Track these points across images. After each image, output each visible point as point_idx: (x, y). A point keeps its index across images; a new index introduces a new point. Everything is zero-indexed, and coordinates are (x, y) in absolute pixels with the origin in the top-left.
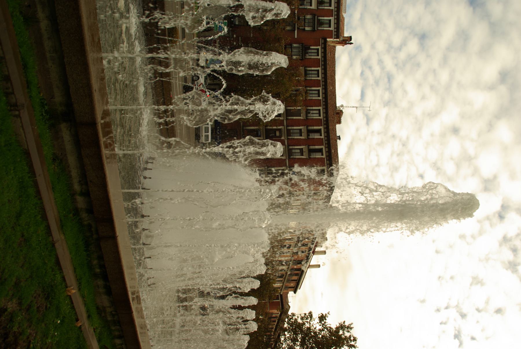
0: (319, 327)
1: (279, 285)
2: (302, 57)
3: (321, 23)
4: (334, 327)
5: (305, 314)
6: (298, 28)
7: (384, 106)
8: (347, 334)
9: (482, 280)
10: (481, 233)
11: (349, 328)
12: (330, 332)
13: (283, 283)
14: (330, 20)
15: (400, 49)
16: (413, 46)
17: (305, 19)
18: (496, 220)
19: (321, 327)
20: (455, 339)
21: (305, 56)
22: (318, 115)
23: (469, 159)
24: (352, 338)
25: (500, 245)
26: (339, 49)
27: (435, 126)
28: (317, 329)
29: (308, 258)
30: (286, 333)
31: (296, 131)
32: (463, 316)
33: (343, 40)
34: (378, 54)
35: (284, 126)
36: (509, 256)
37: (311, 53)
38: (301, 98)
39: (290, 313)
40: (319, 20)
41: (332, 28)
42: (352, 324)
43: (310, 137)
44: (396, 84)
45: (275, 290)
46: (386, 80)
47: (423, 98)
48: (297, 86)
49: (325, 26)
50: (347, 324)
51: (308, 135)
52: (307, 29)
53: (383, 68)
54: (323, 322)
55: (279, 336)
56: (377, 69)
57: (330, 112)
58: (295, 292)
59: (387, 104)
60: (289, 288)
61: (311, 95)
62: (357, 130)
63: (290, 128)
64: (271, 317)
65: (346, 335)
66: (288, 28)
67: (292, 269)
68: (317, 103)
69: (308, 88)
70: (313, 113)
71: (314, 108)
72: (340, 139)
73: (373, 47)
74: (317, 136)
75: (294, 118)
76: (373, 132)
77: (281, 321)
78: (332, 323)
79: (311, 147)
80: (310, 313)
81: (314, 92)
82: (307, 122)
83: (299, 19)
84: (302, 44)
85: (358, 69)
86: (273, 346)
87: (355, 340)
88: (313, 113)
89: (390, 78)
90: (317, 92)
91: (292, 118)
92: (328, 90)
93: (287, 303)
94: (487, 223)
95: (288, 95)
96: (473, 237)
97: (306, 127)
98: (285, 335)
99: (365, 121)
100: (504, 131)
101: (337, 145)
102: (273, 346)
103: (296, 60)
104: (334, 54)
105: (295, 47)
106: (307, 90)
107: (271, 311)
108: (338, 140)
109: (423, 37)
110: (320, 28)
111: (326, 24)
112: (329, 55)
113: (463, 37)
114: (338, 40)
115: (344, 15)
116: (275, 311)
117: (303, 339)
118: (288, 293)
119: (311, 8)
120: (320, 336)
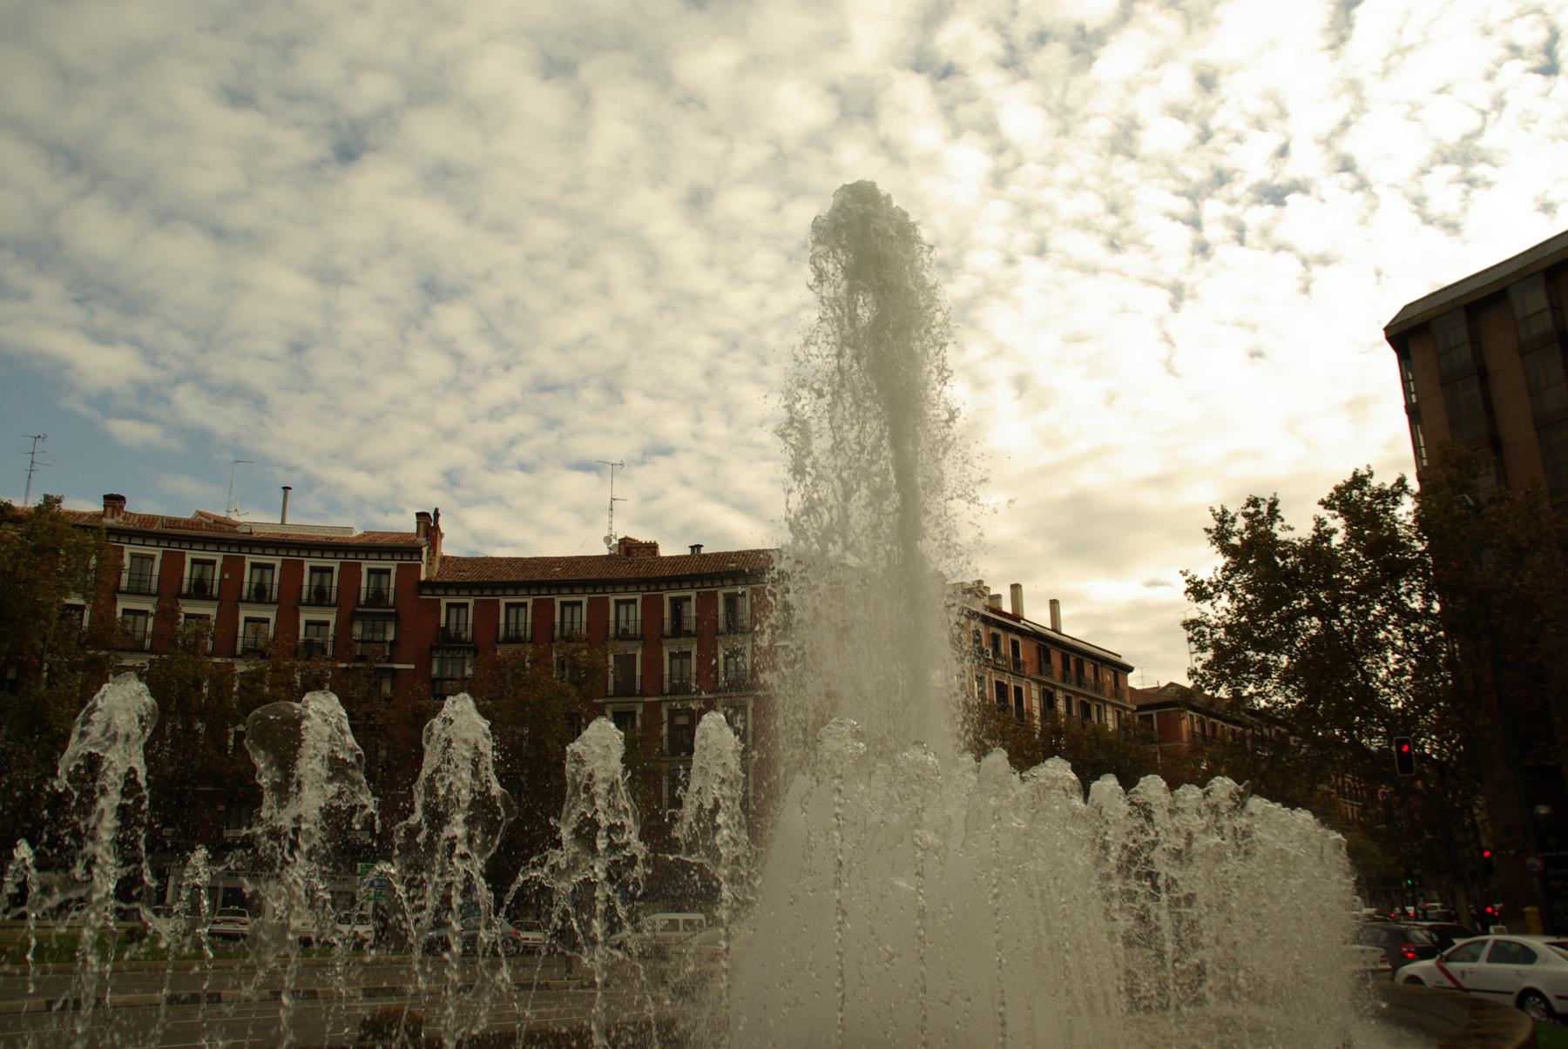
0: (1224, 601)
1: (1109, 716)
2: (469, 649)
3: (377, 597)
4: (1222, 561)
5: (1190, 640)
6: (390, 660)
7: (622, 401)
8: (1241, 523)
9: (1119, 126)
10: (989, 128)
11: (1223, 518)
12: (1234, 571)
13: (1105, 703)
14: (370, 571)
15: (458, 356)
16: (455, 320)
17: (362, 641)
18: (953, 86)
19: (1225, 596)
20: (1283, 204)
21: (465, 641)
22: (632, 607)
23: (781, 158)
24: (1251, 510)
25: (1026, 76)
26: (447, 549)
27: (683, 247)
28: (1229, 606)
29: (1035, 636)
30: (1245, 693)
31: (676, 670)
32: (1221, 178)
33: (427, 535)
34: (473, 420)
35: (660, 703)
36: (1054, 57)
37: (458, 624)
38: (585, 653)
39: (1189, 684)
40: (368, 603)
41: (392, 566)
42: (1212, 510)
43: (693, 628)
44: (560, 369)
45: (1123, 725)
46: (547, 398)
47: (604, 289)
48: (549, 665)
49: (384, 585)
50: (1213, 524)
51: (688, 634)
52: (390, 637)
53: (514, 407)
54: (1211, 589)
55: (1253, 713)
56: (516, 424)
57: (623, 573)
58: (1130, 669)
59: (613, 389)
60: (1119, 688)
61: (577, 626)
62: (686, 483)
63: (666, 686)
64: (1203, 740)
65: (1243, 527)
66: (387, 688)
67: (1064, 679)
68: (599, 608)
69: (557, 632)
70: (627, 621)
71: (612, 617)
72: (699, 547)
73: (451, 435)
74: (691, 610)
75: (638, 672)
76: (694, 436)
77: (1210, 708)
78: (1210, 564)
79: (721, 625)
80: (1188, 625)
81: (568, 618)
82: (651, 637)
83: (362, 658)
84: (432, 649)
85: (513, 481)
86: (1283, 731)
87: (1254, 502)
88: (627, 621)
89: (544, 386)
90: (568, 610)
91: (638, 679)
92: (562, 577)
93: (1158, 690)
94: (963, 112)
95: (573, 691)
96: (1000, 150)
97: (664, 641)
98: (1251, 695)
99: (660, 459)
100: (708, 62)
101: (717, 555)
102: (1283, 731)
103: (475, 667)
104: (465, 560)
105: (441, 668)
106: (562, 637)
107: (1185, 738)
108: (703, 551)
109: (434, 290)
110: (391, 599)
111: (379, 581)
112: (467, 576)
113: (442, 178)
114: (425, 550)
115: (358, 532)
116: (1185, 725)
117: (1259, 646)
118: (1132, 689)
119: (333, 623)
120: (1249, 597)
